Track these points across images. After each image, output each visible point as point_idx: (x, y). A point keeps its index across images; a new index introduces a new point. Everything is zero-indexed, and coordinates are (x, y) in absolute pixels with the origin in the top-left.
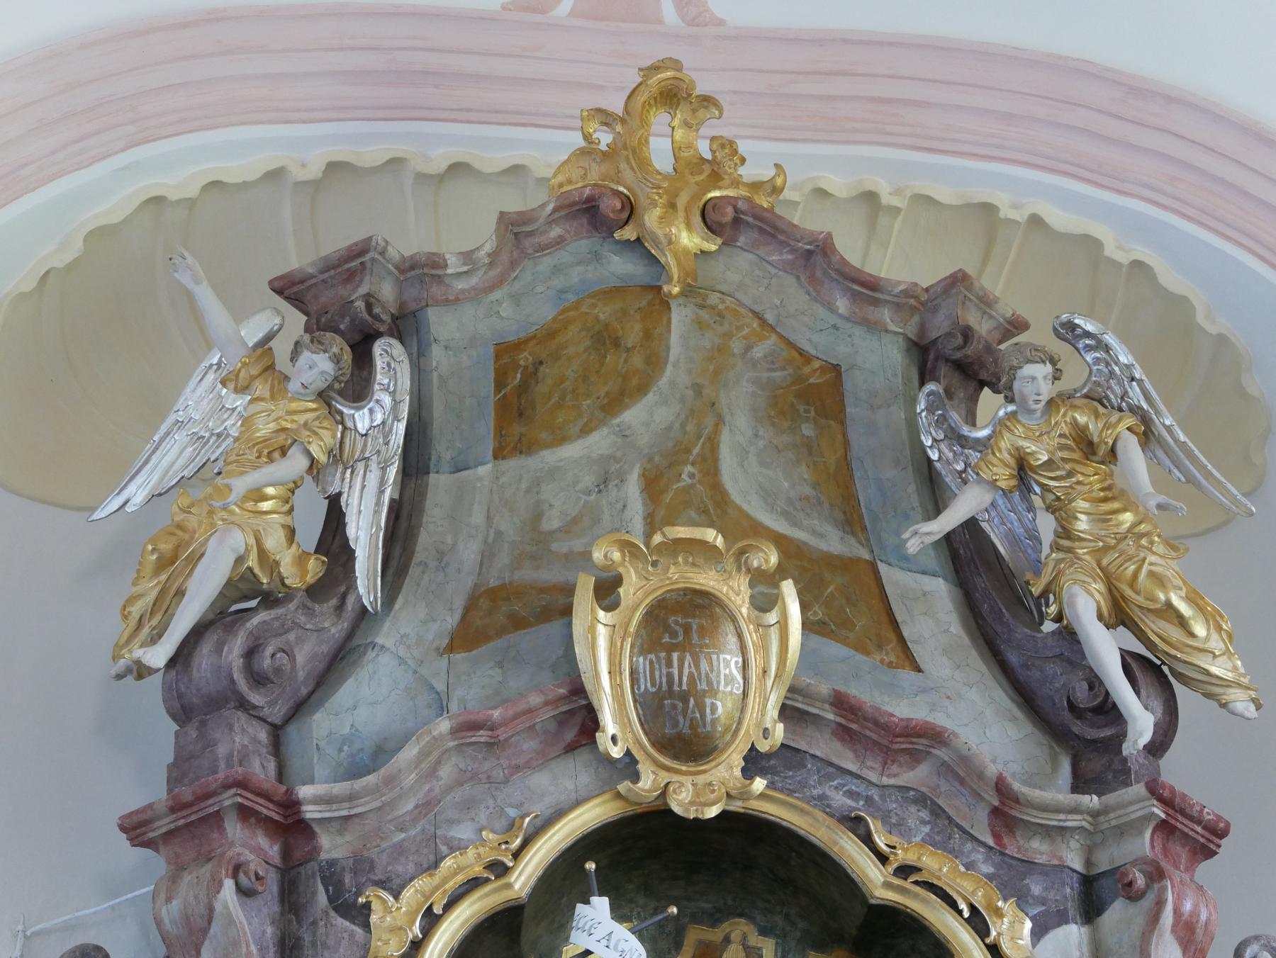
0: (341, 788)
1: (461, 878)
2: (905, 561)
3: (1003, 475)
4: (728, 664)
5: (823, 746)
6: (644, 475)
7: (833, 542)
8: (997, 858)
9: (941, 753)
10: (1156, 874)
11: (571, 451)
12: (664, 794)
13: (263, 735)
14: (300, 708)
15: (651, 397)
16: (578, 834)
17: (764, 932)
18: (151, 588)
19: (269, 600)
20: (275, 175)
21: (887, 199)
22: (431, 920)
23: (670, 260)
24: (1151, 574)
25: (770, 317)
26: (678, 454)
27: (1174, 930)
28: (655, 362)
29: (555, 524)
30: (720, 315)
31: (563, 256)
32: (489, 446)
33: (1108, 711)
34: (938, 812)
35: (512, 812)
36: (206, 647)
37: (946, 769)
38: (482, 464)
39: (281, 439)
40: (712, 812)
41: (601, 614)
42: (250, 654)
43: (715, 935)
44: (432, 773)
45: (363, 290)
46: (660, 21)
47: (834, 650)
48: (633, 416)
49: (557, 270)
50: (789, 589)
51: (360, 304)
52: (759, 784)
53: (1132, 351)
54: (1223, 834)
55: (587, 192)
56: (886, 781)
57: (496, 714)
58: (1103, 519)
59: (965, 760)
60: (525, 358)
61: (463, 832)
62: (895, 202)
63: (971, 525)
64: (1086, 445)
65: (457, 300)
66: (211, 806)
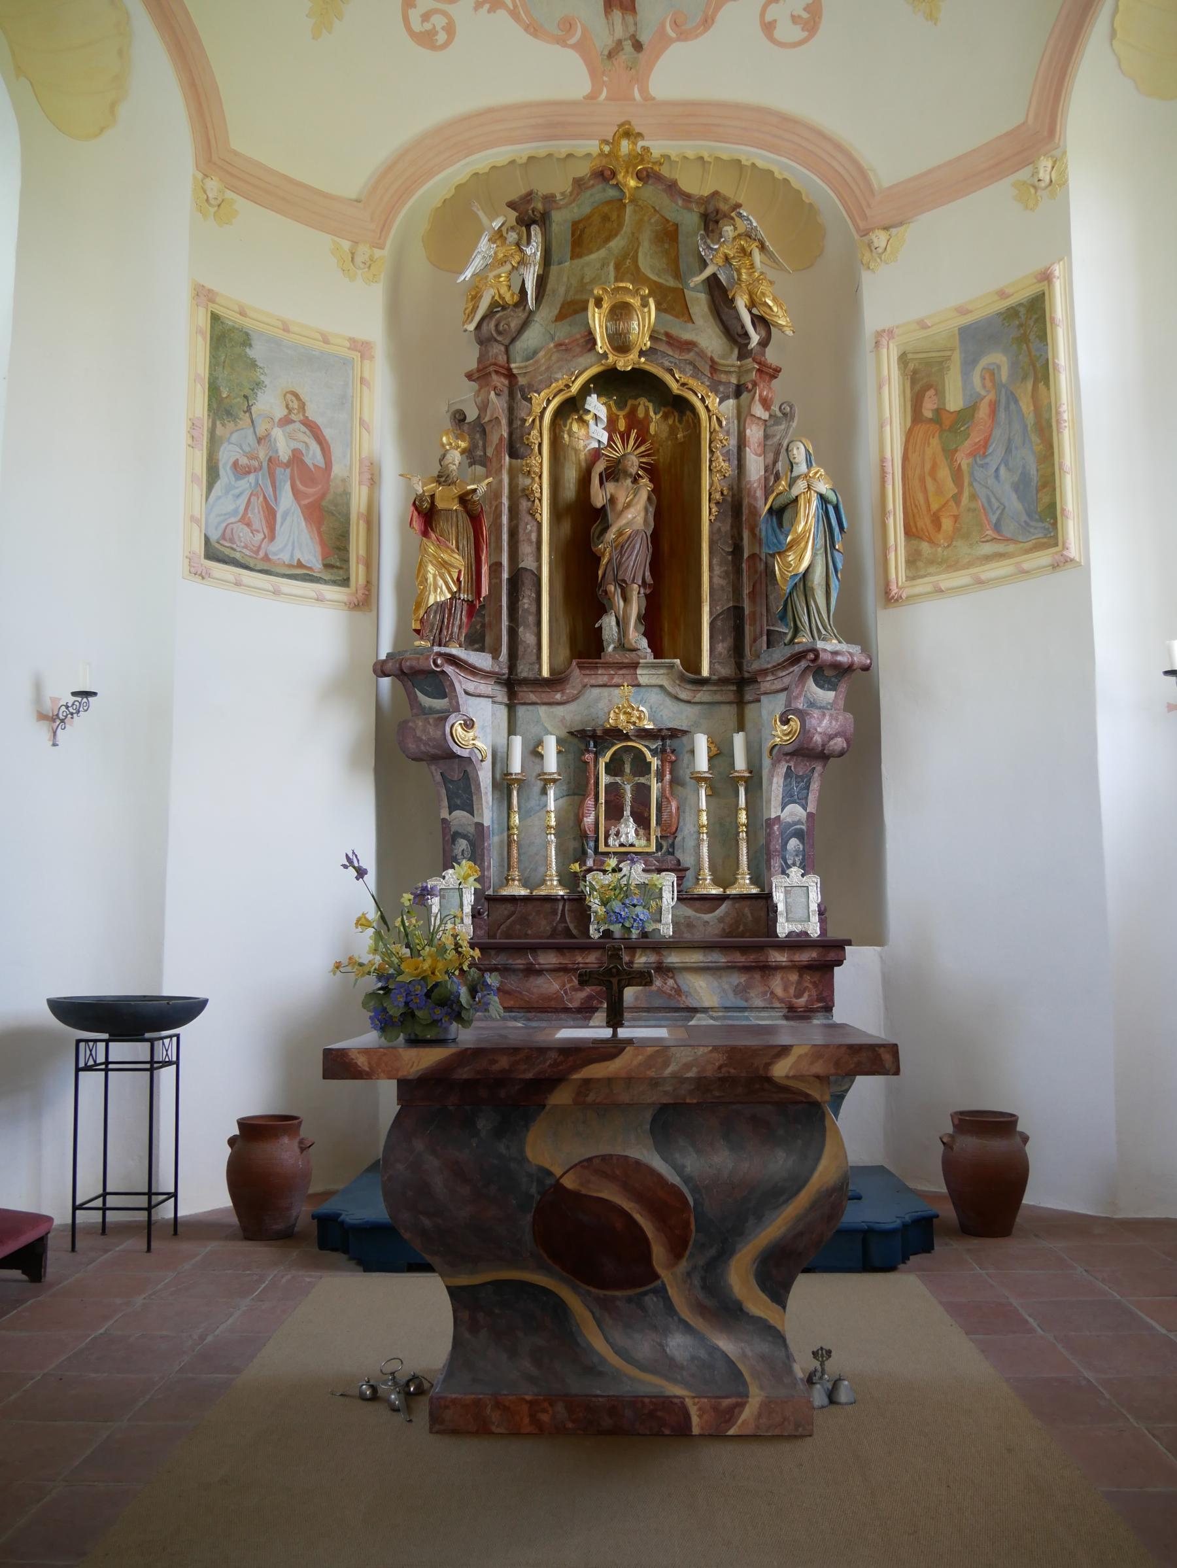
0: (522, 364)
1: (557, 389)
2: (694, 289)
3: (720, 261)
5: (663, 347)
6: (615, 263)
7: (671, 283)
8: (711, 380)
9: (695, 349)
10: (755, 384)
11: (593, 256)
12: (615, 363)
13: (503, 348)
14: (513, 340)
15: (618, 237)
16: (591, 375)
17: (649, 401)
18: (470, 305)
19: (504, 308)
20: (513, 162)
21: (707, 158)
22: (549, 402)
23: (626, 191)
24: (762, 292)
25: (657, 208)
26: (625, 256)
27: (759, 400)
28: (620, 225)
29: (588, 281)
30: (642, 208)
32: (569, 255)
33: (746, 335)
34: (695, 367)
35: (572, 370)
36: (485, 324)
37: (698, 354)
38: (566, 262)
39: (505, 259)
40: (629, 368)
41: (596, 310)
42: (497, 326)
43: (636, 402)
44: (550, 358)
45: (532, 206)
46: (635, 100)
47: (669, 317)
50: (651, 301)
51: (530, 212)
52: (643, 360)
53: (757, 222)
54: (779, 371)
55: (600, 169)
56: (680, 358)
57: (567, 341)
58: (750, 275)
59: (702, 351)
60: (581, 226)
61: (559, 376)
62: (709, 160)
63: (714, 275)
65: (560, 208)
66: (488, 370)
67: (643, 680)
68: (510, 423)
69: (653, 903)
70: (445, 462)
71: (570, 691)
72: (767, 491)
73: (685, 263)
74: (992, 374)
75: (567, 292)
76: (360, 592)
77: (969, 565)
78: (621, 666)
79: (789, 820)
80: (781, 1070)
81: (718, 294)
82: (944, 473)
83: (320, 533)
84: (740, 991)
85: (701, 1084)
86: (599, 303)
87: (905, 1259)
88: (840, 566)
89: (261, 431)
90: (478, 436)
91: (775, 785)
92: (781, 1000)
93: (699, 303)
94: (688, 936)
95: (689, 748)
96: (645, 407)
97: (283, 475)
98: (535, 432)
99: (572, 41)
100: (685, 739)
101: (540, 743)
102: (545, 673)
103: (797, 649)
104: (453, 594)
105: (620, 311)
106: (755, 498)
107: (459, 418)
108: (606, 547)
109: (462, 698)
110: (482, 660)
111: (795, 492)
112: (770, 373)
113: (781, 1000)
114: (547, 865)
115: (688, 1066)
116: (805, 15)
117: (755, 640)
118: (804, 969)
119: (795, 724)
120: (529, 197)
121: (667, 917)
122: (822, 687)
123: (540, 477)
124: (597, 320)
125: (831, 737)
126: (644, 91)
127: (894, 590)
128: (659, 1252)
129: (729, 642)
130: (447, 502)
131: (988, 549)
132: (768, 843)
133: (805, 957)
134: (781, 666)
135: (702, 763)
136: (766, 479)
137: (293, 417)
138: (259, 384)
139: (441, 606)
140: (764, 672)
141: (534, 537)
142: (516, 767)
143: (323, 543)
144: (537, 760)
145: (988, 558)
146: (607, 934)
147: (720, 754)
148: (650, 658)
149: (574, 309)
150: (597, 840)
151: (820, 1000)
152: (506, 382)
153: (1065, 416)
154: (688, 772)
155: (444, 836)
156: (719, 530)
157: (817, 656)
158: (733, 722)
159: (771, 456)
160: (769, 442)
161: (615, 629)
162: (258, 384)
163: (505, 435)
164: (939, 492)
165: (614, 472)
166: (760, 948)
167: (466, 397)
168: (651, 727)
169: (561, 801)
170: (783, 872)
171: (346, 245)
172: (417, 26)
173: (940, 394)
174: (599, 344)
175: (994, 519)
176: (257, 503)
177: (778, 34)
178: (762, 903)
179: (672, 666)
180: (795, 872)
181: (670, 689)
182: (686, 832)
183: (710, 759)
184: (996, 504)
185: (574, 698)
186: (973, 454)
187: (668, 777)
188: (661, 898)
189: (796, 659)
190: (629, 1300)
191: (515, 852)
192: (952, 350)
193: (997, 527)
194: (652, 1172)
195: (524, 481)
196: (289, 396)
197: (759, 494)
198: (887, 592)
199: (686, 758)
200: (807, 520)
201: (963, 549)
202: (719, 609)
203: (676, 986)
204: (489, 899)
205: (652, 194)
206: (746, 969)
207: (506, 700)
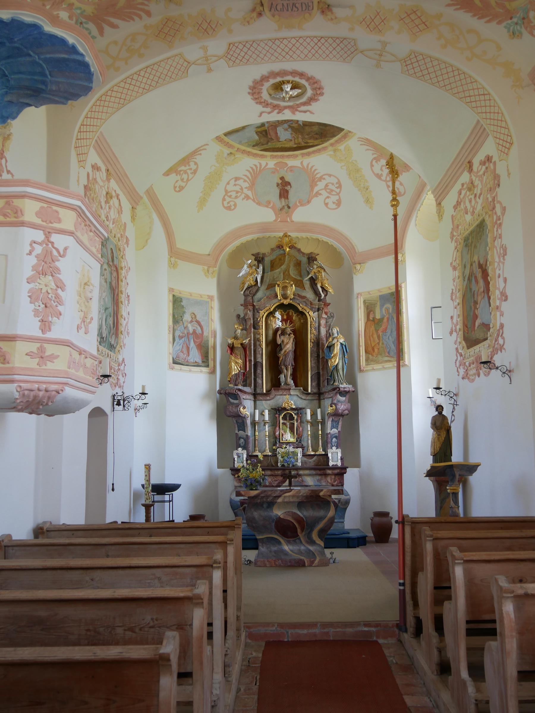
4: (289, 292)
5: (297, 297)
7: (299, 278)
10: (323, 309)
14: (254, 295)
18: (242, 285)
20: (253, 239)
22: (265, 313)
28: (284, 261)
31: (277, 251)
36: (246, 292)
37: (307, 300)
47: (298, 288)
48: (282, 267)
49: (276, 253)
60: (273, 262)
61: (267, 305)
63: (312, 277)
64: (319, 271)
67: (292, 393)
68: (254, 319)
69: (295, 457)
70: (236, 333)
71: (272, 396)
72: (327, 340)
73: (304, 272)
74: (388, 310)
75: (269, 281)
76: (212, 369)
77: (381, 363)
78: (286, 389)
79: (333, 433)
80: (321, 494)
81: (313, 281)
82: (375, 336)
83: (201, 354)
84: (318, 481)
85: (307, 497)
86: (278, 285)
87: (358, 546)
88: (346, 362)
89: (185, 325)
90: (244, 322)
91: (329, 424)
92: (330, 483)
93: (307, 284)
94: (305, 466)
95: (305, 412)
96: (291, 312)
97: (191, 337)
98: (261, 322)
99: (270, 206)
100: (304, 410)
101: (263, 411)
102: (265, 391)
103: (334, 387)
104: (239, 371)
105: (285, 288)
106: (323, 341)
107: (238, 316)
108: (281, 355)
109: (242, 400)
110: (247, 389)
111: (334, 342)
112: (327, 305)
113: (330, 483)
114: (266, 447)
115: (304, 493)
116: (337, 202)
117: (323, 382)
118: (336, 475)
119: (334, 407)
120: (258, 254)
121: (299, 461)
122: (341, 397)
123: (262, 335)
124: (278, 290)
125: (344, 411)
126: (291, 219)
127: (362, 368)
128: (299, 530)
129: (316, 382)
130: (237, 344)
131: (386, 359)
132: (327, 440)
133: (336, 471)
134: (330, 391)
135: (309, 417)
136: (326, 334)
137: (193, 320)
138: (184, 312)
139: (236, 374)
140: (326, 392)
141: (261, 352)
142: (257, 419)
143: (202, 356)
144: (262, 416)
145: (387, 361)
146: (283, 465)
147: (314, 414)
148: (294, 387)
149: (271, 286)
150: (280, 439)
151: (340, 483)
152: (252, 307)
153: (405, 326)
154: (305, 419)
155: (236, 437)
156: (313, 350)
157: (339, 389)
158: (317, 405)
159: (328, 328)
160: (327, 324)
161: (284, 378)
162: (184, 312)
163: (252, 322)
164: (374, 341)
165: (283, 333)
166: (324, 469)
167: (241, 311)
168: (294, 407)
169: (269, 428)
170: (331, 448)
171: (206, 268)
172: (226, 205)
173: (374, 313)
174: (279, 297)
175: (388, 350)
176: (185, 346)
177: (329, 206)
178: (326, 456)
179: (300, 389)
180: (334, 448)
181: (300, 396)
182: (304, 436)
183: (311, 416)
184: (388, 347)
185: (273, 398)
186: (382, 332)
187: (299, 421)
188: (298, 455)
189: (334, 389)
190: (293, 541)
191: (257, 442)
192: (377, 301)
193: (389, 353)
194: (298, 514)
195: (258, 336)
196: (192, 314)
197: (325, 339)
198: (360, 368)
199: (304, 415)
200: (337, 349)
201: (380, 358)
202: (313, 373)
204: (250, 456)
205: (294, 252)
206: (320, 475)
207: (253, 399)
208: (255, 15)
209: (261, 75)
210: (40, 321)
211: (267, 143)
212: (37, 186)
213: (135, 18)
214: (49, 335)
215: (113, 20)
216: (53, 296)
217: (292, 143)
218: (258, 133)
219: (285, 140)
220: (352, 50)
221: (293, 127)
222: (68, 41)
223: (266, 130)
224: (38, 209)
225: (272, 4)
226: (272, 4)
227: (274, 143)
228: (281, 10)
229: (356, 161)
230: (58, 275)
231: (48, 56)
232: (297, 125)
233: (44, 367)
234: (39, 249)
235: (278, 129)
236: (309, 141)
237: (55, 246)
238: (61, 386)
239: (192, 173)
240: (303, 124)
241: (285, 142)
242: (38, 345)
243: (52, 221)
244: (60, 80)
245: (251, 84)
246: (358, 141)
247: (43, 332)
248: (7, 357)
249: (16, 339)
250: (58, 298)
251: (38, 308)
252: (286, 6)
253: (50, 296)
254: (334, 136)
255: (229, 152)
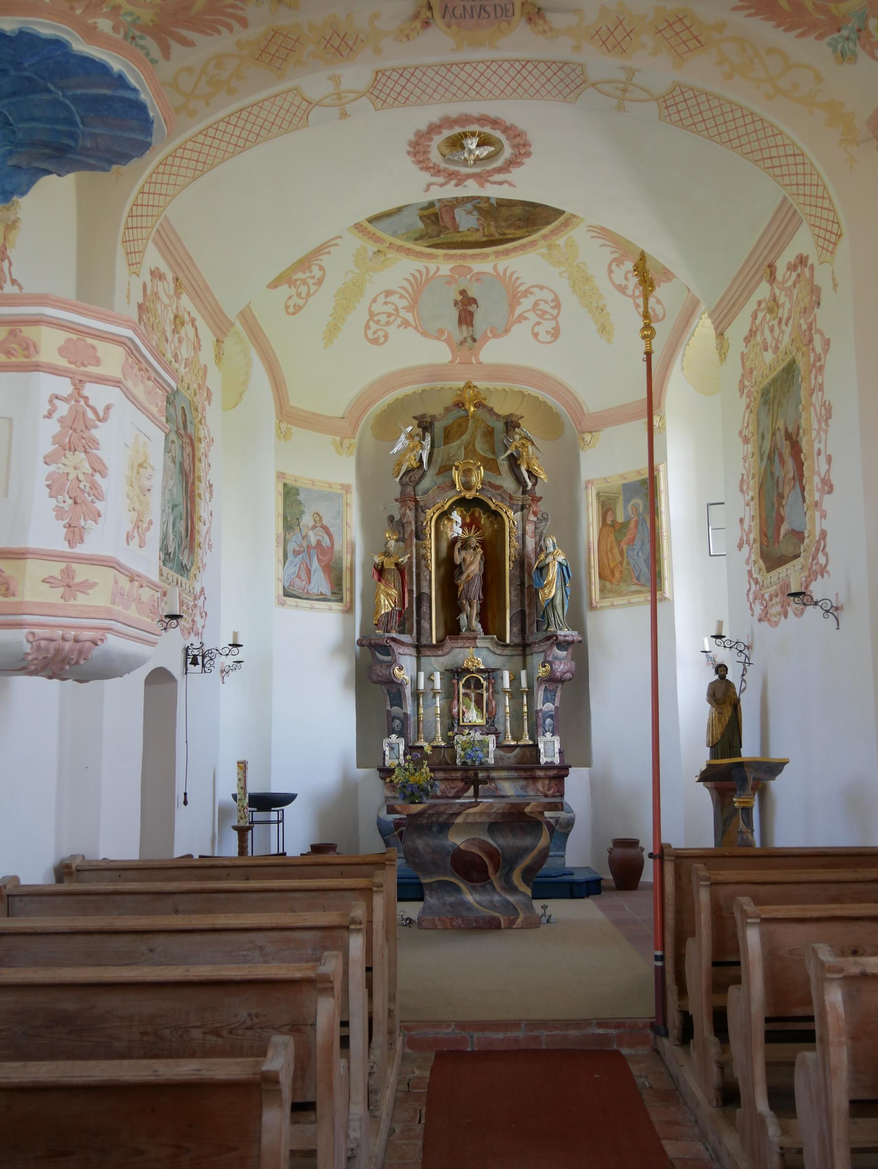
4: (474, 478)
5: (487, 487)
7: (491, 456)
10: (530, 506)
14: (417, 484)
18: (397, 468)
20: (415, 392)
22: (434, 513)
28: (467, 428)
31: (454, 412)
36: (404, 478)
37: (503, 491)
47: (489, 473)
48: (463, 438)
49: (453, 414)
60: (448, 429)
61: (438, 501)
63: (512, 453)
64: (523, 444)
67: (479, 645)
68: (416, 523)
69: (485, 749)
70: (388, 546)
71: (446, 650)
72: (537, 558)
73: (498, 446)
74: (636, 508)
75: (442, 460)
76: (348, 605)
77: (626, 595)
78: (469, 638)
79: (546, 710)
80: (527, 810)
81: (514, 461)
82: (616, 551)
83: (330, 580)
84: (522, 788)
85: (503, 815)
86: (457, 468)
87: (588, 896)
88: (569, 594)
89: (304, 533)
90: (400, 528)
91: (540, 695)
92: (542, 792)
93: (504, 466)
94: (500, 764)
95: (500, 676)
96: (478, 512)
97: (314, 552)
98: (428, 528)
99: (443, 338)
100: (499, 672)
101: (432, 674)
102: (434, 642)
103: (549, 634)
104: (393, 608)
105: (467, 472)
106: (530, 558)
107: (391, 518)
108: (462, 581)
109: (398, 656)
110: (405, 638)
111: (547, 561)
112: (536, 500)
113: (542, 792)
114: (436, 732)
115: (499, 809)
116: (552, 331)
117: (531, 626)
118: (551, 778)
119: (548, 667)
120: (424, 416)
121: (491, 755)
122: (560, 650)
123: (431, 549)
124: (456, 475)
125: (565, 673)
126: (477, 359)
127: (594, 603)
128: (490, 870)
129: (519, 626)
130: (389, 564)
131: (634, 588)
132: (537, 721)
133: (552, 773)
134: (542, 641)
135: (507, 684)
136: (536, 548)
137: (317, 525)
138: (302, 512)
139: (387, 614)
140: (535, 643)
141: (428, 577)
142: (422, 686)
143: (331, 584)
144: (431, 682)
145: (634, 592)
146: (464, 763)
147: (515, 679)
148: (482, 635)
149: (445, 469)
150: (459, 720)
151: (558, 792)
152: (414, 504)
153: (664, 534)
154: (500, 687)
155: (388, 717)
156: (514, 574)
157: (557, 638)
158: (521, 664)
159: (538, 537)
160: (537, 531)
161: (466, 620)
162: (302, 512)
163: (414, 529)
164: (614, 559)
165: (465, 545)
166: (532, 769)
167: (395, 510)
168: (483, 667)
169: (442, 701)
170: (544, 735)
171: (338, 439)
172: (371, 336)
173: (614, 513)
174: (458, 486)
175: (637, 574)
176: (303, 567)
177: (540, 338)
178: (534, 748)
179: (493, 639)
180: (548, 734)
181: (492, 649)
182: (499, 715)
183: (510, 681)
184: (638, 568)
185: (448, 653)
186: (628, 544)
187: (491, 690)
188: (488, 747)
189: (548, 638)
190: (481, 886)
191: (421, 725)
192: (619, 494)
193: (638, 578)
194: (488, 843)
195: (423, 551)
196: (315, 515)
197: (533, 556)
198: (591, 604)
199: (499, 681)
200: (553, 572)
201: (623, 587)
202: (514, 611)
203: (289, 1027)
204: (411, 747)
205: (482, 414)
206: (526, 778)
207: (416, 654)
208: (418, 24)
209: (428, 123)
210: (65, 527)
211: (439, 235)
212: (61, 305)
213: (222, 29)
214: (80, 550)
215: (185, 33)
216: (88, 485)
217: (480, 234)
218: (423, 218)
219: (468, 230)
220: (578, 81)
221: (482, 208)
222: (112, 68)
223: (437, 213)
224: (62, 342)
225: (446, 6)
226: (446, 6)
227: (450, 235)
228: (461, 17)
229: (584, 264)
230: (95, 451)
231: (79, 92)
232: (487, 205)
233: (72, 602)
234: (63, 409)
235: (457, 211)
236: (507, 231)
237: (91, 403)
238: (100, 632)
239: (315, 284)
240: (497, 203)
241: (467, 233)
242: (63, 566)
243: (86, 362)
244: (98, 131)
245: (412, 138)
246: (588, 231)
247: (71, 544)
248: (11, 586)
249: (26, 556)
250: (96, 489)
251: (62, 505)
252: (469, 9)
253: (81, 486)
254: (548, 223)
255: (375, 249)
